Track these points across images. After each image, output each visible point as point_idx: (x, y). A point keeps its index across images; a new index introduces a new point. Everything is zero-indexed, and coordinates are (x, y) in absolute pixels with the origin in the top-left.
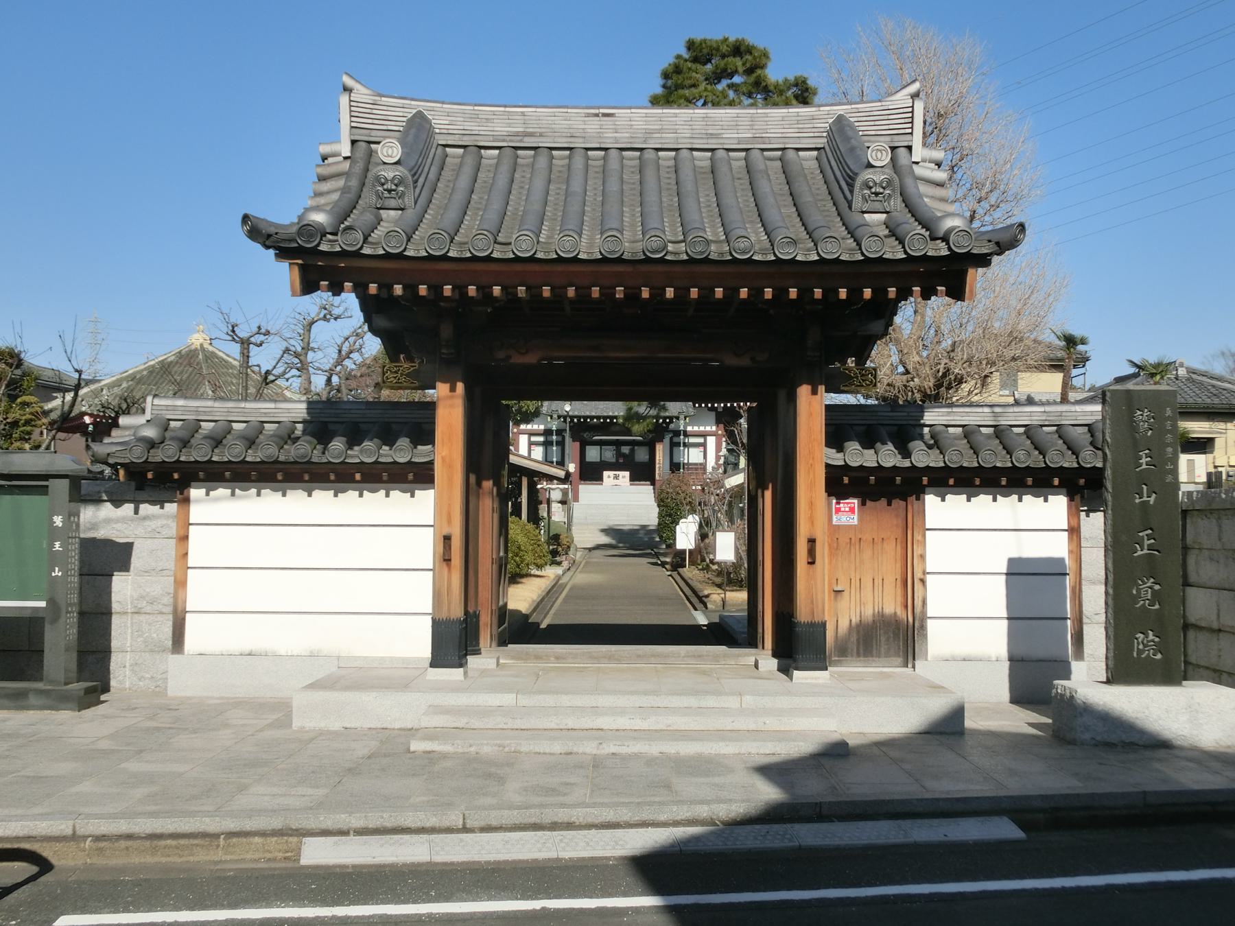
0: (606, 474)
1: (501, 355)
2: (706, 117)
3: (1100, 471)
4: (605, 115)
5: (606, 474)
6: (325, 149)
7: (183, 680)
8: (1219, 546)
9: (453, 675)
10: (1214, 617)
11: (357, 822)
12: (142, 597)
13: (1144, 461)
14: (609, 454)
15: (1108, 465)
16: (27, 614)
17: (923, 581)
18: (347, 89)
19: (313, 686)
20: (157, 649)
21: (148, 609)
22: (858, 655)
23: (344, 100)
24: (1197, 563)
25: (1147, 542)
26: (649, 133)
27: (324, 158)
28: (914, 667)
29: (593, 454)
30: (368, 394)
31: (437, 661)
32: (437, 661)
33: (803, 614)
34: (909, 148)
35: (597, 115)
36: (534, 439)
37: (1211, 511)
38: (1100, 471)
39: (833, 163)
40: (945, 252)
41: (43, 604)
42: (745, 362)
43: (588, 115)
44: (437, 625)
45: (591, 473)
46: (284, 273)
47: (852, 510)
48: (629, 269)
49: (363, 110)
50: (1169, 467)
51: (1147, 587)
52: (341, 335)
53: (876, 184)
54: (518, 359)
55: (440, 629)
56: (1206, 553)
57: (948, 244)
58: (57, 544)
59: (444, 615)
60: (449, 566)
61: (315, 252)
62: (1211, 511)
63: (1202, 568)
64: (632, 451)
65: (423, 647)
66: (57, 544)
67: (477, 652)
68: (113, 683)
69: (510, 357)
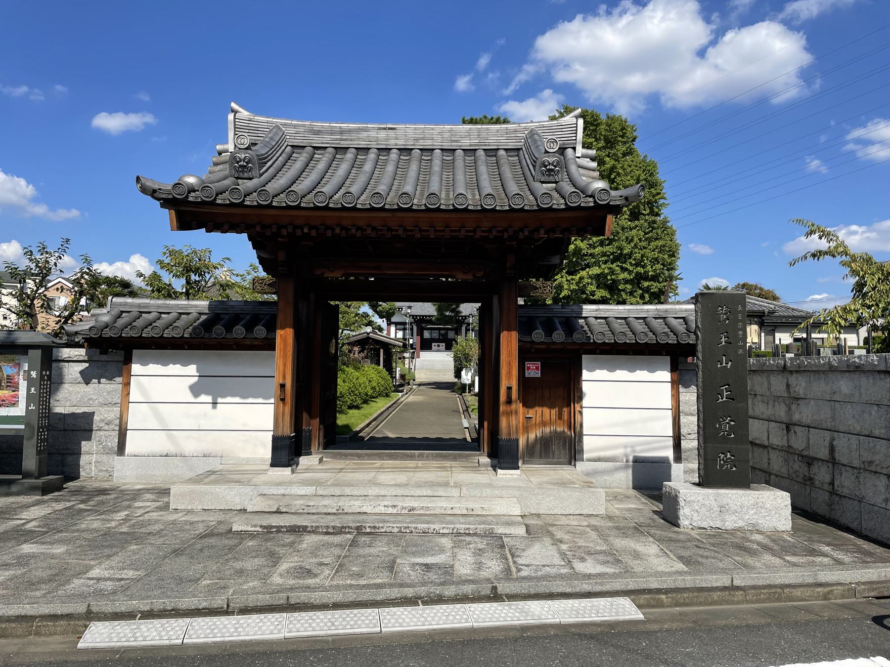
0: (433, 344)
1: (318, 272)
2: (451, 131)
3: (694, 346)
4: (390, 129)
5: (433, 344)
6: (219, 147)
7: (125, 473)
8: (768, 394)
9: (285, 472)
10: (765, 438)
11: (145, 606)
12: (103, 420)
13: (723, 340)
14: (435, 335)
15: (699, 342)
16: (13, 433)
17: (581, 413)
18: (235, 112)
19: (197, 480)
20: (107, 451)
21: (106, 427)
22: (541, 457)
23: (231, 117)
24: (753, 404)
25: (725, 394)
26: (417, 140)
27: (220, 154)
28: (575, 465)
29: (427, 335)
30: (248, 297)
31: (276, 463)
32: (276, 463)
33: (504, 434)
34: (574, 149)
35: (385, 129)
36: (398, 327)
37: (763, 371)
38: (694, 346)
39: (526, 156)
40: (592, 204)
41: (23, 427)
42: (469, 277)
43: (380, 129)
44: (275, 439)
45: (426, 345)
46: (166, 216)
47: (537, 368)
48: (389, 215)
49: (241, 124)
50: (741, 344)
51: (727, 424)
52: (235, 260)
53: (549, 164)
54: (329, 275)
55: (278, 443)
56: (759, 397)
57: (594, 198)
58: (33, 389)
59: (280, 433)
60: (284, 404)
61: (185, 202)
62: (763, 371)
63: (758, 408)
64: (447, 333)
65: (267, 453)
66: (33, 389)
67: (309, 454)
68: (82, 473)
69: (323, 273)
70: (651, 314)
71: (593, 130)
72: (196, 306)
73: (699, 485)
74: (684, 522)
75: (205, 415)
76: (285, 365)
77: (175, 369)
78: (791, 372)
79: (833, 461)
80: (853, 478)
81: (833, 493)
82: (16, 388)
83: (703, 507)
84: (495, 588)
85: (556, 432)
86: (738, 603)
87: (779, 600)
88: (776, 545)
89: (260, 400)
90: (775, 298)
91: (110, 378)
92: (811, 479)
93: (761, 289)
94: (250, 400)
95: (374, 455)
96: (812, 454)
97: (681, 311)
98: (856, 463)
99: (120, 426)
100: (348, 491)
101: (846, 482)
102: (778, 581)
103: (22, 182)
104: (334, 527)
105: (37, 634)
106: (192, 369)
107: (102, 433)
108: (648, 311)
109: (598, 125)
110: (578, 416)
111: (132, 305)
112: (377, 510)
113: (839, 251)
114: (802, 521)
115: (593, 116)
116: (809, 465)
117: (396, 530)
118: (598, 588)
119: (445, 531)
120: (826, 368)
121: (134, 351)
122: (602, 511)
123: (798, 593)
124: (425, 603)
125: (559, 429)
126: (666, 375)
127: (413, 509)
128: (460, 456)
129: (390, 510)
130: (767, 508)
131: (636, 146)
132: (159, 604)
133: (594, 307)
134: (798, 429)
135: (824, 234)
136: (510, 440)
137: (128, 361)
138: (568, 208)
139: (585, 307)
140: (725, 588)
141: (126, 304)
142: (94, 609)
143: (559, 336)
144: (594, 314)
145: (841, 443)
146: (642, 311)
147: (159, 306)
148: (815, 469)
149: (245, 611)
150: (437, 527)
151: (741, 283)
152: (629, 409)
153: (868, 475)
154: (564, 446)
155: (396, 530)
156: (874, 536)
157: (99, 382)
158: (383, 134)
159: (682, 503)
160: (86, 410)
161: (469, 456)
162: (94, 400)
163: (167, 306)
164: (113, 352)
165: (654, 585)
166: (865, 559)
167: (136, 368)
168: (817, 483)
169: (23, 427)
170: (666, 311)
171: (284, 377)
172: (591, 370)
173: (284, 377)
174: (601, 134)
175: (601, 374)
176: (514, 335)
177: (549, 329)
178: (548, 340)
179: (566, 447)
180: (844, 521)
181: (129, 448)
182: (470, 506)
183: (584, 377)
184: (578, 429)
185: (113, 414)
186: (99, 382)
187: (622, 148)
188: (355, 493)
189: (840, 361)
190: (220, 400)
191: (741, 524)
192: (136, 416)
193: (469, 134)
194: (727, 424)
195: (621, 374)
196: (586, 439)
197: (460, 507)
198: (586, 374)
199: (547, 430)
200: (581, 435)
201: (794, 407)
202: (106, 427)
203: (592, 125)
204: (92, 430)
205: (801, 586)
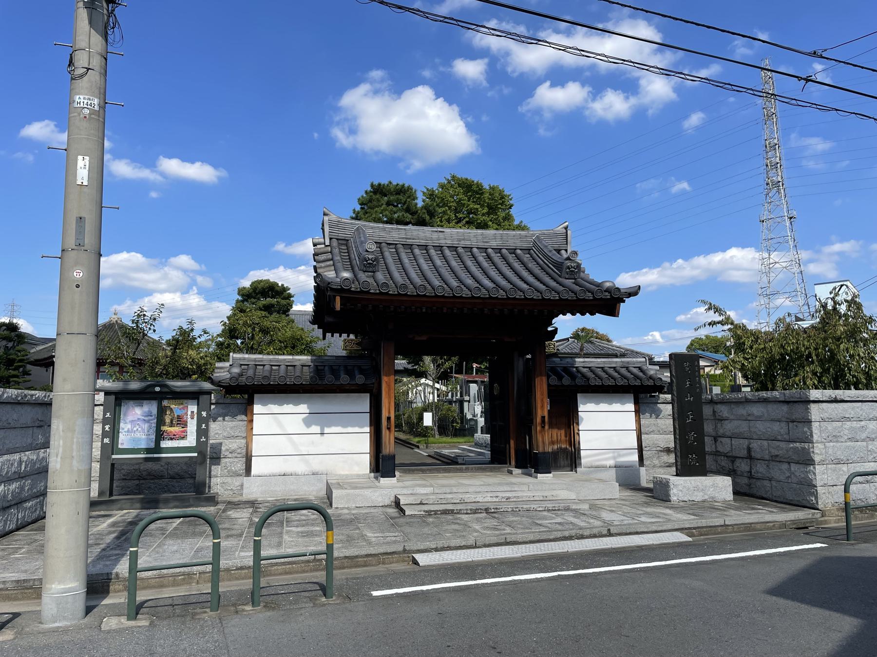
17: (578, 434)
21: (230, 455)
26: (459, 240)
41: (196, 455)
51: (692, 435)
54: (418, 338)
70: (618, 365)
71: (479, 198)
72: (299, 360)
73: (677, 475)
74: (674, 498)
75: (313, 443)
76: (389, 403)
77: (288, 408)
78: (716, 403)
79: (750, 457)
80: (765, 467)
81: (751, 477)
82: (185, 425)
83: (684, 488)
84: (609, 530)
85: (561, 448)
86: (730, 533)
87: (749, 531)
88: (727, 506)
89: (357, 429)
90: (609, 341)
91: (234, 416)
92: (734, 471)
93: (597, 333)
94: (350, 430)
95: (434, 469)
96: (734, 454)
97: (638, 362)
98: (767, 457)
99: (247, 454)
100: (455, 490)
101: (760, 468)
102: (747, 521)
103: (139, 255)
104: (471, 510)
105: (384, 563)
106: (303, 408)
107: (227, 460)
108: (616, 362)
109: (482, 194)
110: (576, 436)
111: (249, 360)
112: (485, 500)
113: (728, 321)
114: (737, 497)
115: (478, 186)
116: (733, 462)
117: (510, 510)
118: (660, 528)
119: (541, 509)
120: (743, 400)
121: (256, 396)
122: (617, 497)
123: (758, 526)
124: (578, 538)
125: (563, 446)
126: (631, 407)
127: (509, 498)
128: (494, 468)
129: (495, 499)
130: (720, 487)
131: (513, 211)
132: (440, 545)
133: (581, 360)
134: (724, 440)
135: (717, 310)
136: (544, 453)
137: (251, 403)
138: (595, 299)
139: (577, 360)
140: (722, 526)
141: (244, 359)
142: (407, 548)
143: (566, 381)
144: (582, 365)
145: (755, 445)
146: (613, 362)
147: (270, 360)
148: (738, 462)
149: (485, 546)
150: (535, 506)
151: (581, 327)
152: (606, 429)
153: (774, 463)
154: (567, 458)
155: (510, 510)
156: (782, 500)
157: (224, 420)
158: (435, 236)
159: (672, 486)
160: (218, 441)
161: (500, 468)
162: (219, 435)
163: (278, 360)
164: (242, 395)
165: (687, 526)
166: (783, 510)
167: (257, 408)
168: (739, 473)
169: (196, 455)
170: (628, 363)
171: (389, 412)
172: (584, 404)
173: (389, 412)
174: (484, 201)
175: (590, 406)
176: (544, 379)
177: (560, 378)
178: (560, 384)
179: (569, 458)
180: (759, 494)
181: (254, 471)
182: (545, 494)
183: (580, 409)
184: (577, 446)
185: (237, 444)
186: (224, 420)
187: (502, 214)
188: (460, 491)
189: (753, 395)
190: (327, 430)
191: (706, 497)
192: (258, 446)
193: (495, 237)
194: (692, 435)
195: (603, 406)
196: (583, 453)
197: (539, 495)
198: (581, 408)
199: (556, 447)
200: (579, 450)
201: (719, 425)
202: (230, 455)
203: (478, 193)
204: (219, 458)
205: (757, 523)
